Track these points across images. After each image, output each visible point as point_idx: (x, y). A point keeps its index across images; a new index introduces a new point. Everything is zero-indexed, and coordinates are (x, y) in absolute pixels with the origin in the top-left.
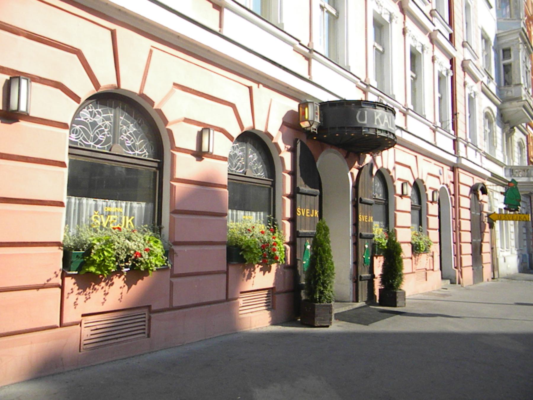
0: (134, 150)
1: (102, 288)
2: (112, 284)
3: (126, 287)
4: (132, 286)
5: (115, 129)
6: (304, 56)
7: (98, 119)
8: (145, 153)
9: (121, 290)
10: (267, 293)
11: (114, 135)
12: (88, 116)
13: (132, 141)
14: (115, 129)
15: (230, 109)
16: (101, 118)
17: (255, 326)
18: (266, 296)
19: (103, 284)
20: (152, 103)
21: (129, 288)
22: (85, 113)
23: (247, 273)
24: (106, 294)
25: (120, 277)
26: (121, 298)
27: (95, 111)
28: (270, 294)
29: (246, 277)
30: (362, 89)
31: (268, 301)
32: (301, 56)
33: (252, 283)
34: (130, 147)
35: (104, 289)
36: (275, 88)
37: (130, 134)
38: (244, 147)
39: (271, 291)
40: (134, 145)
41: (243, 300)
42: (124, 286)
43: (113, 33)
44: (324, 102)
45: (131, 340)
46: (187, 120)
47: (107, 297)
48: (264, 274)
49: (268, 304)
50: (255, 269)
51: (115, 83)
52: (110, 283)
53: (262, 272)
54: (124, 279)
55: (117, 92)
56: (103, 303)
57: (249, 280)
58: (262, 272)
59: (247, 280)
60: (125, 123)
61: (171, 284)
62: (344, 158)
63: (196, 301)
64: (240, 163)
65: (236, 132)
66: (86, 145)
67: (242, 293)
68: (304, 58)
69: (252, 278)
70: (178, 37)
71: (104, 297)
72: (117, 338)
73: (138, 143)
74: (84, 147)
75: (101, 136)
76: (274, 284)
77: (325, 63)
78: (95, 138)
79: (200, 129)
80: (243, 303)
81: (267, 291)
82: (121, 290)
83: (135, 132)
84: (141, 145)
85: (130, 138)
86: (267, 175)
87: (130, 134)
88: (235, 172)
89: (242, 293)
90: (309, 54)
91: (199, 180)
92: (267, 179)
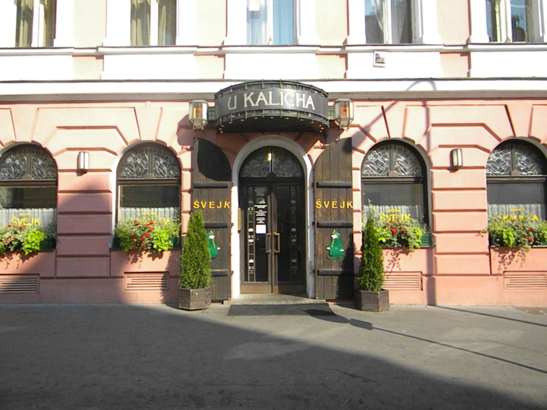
0: (527, 171)
1: (6, 260)
2: (12, 259)
3: (21, 261)
4: (155, 258)
5: (513, 162)
6: (215, 55)
7: (379, 159)
8: (536, 172)
9: (18, 263)
10: (162, 276)
11: (390, 165)
12: (495, 157)
13: (525, 166)
14: (513, 162)
15: (482, 128)
16: (503, 156)
17: (142, 301)
18: (161, 278)
19: (6, 258)
20: (413, 142)
21: (23, 261)
22: (371, 157)
23: (132, 258)
24: (8, 264)
25: (17, 254)
26: (18, 267)
27: (498, 153)
28: (166, 277)
29: (131, 261)
30: (338, 53)
31: (164, 283)
32: (213, 56)
33: (139, 266)
34: (523, 170)
35: (6, 261)
36: (416, 97)
37: (524, 162)
38: (509, 153)
39: (166, 274)
40: (527, 168)
41: (133, 279)
42: (20, 260)
43: (506, 107)
44: (217, 93)
45: (14, 293)
46: (441, 146)
47: (9, 266)
48: (153, 259)
49: (163, 285)
50: (140, 256)
51: (512, 134)
52: (10, 258)
53: (151, 258)
54: (19, 256)
55: (515, 138)
56: (6, 269)
57: (134, 264)
58: (151, 258)
59: (132, 263)
60: (518, 156)
61: (56, 262)
62: (293, 141)
63: (79, 275)
64: (128, 170)
65: (492, 144)
66: (495, 174)
67: (126, 273)
68: (216, 57)
69: (138, 262)
70: (448, 92)
71: (7, 265)
72: (18, 291)
73: (529, 167)
74: (494, 176)
75: (382, 168)
76: (166, 269)
77: (273, 51)
78: (500, 168)
79: (451, 149)
80: (133, 282)
81: (163, 274)
82: (18, 263)
83: (526, 160)
84: (532, 167)
85: (523, 164)
86: (540, 172)
87: (524, 162)
88: (378, 175)
89: (126, 273)
90: (220, 51)
91: (82, 189)
92: (541, 175)
